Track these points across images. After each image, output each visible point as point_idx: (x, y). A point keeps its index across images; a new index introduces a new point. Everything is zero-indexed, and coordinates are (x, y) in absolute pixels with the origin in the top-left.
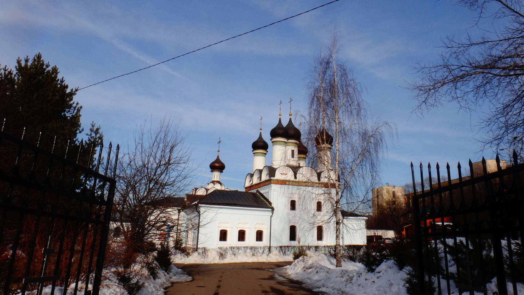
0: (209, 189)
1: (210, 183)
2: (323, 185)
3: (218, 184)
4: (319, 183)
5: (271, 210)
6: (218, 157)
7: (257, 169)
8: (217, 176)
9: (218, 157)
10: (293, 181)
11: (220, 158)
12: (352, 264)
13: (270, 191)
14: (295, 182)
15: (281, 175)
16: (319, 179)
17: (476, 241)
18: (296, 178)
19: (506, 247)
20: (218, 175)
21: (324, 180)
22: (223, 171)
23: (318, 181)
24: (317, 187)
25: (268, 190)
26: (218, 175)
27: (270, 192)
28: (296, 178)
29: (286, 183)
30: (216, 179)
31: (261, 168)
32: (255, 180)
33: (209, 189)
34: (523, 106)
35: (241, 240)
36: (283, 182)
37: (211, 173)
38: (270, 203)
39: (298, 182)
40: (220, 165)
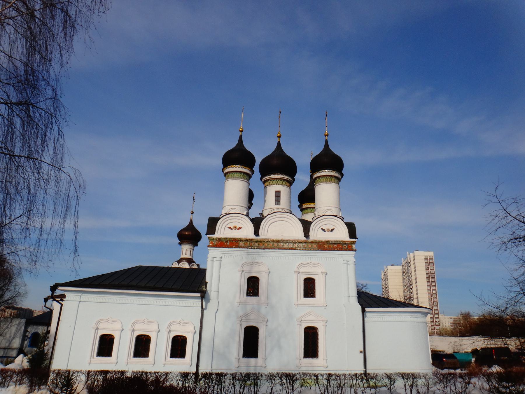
2: (315, 246)
4: (305, 242)
5: (199, 295)
6: (191, 221)
8: (187, 250)
9: (191, 221)
10: (252, 241)
11: (194, 223)
12: (25, 264)
14: (257, 241)
15: (230, 230)
16: (307, 233)
17: (495, 357)
18: (256, 233)
19: (453, 339)
20: (188, 249)
21: (316, 234)
22: (198, 243)
23: (305, 239)
24: (404, 279)
26: (188, 249)
28: (256, 233)
29: (238, 244)
30: (184, 256)
34: (1, 12)
35: (179, 356)
36: (234, 243)
37: (179, 246)
39: (262, 241)
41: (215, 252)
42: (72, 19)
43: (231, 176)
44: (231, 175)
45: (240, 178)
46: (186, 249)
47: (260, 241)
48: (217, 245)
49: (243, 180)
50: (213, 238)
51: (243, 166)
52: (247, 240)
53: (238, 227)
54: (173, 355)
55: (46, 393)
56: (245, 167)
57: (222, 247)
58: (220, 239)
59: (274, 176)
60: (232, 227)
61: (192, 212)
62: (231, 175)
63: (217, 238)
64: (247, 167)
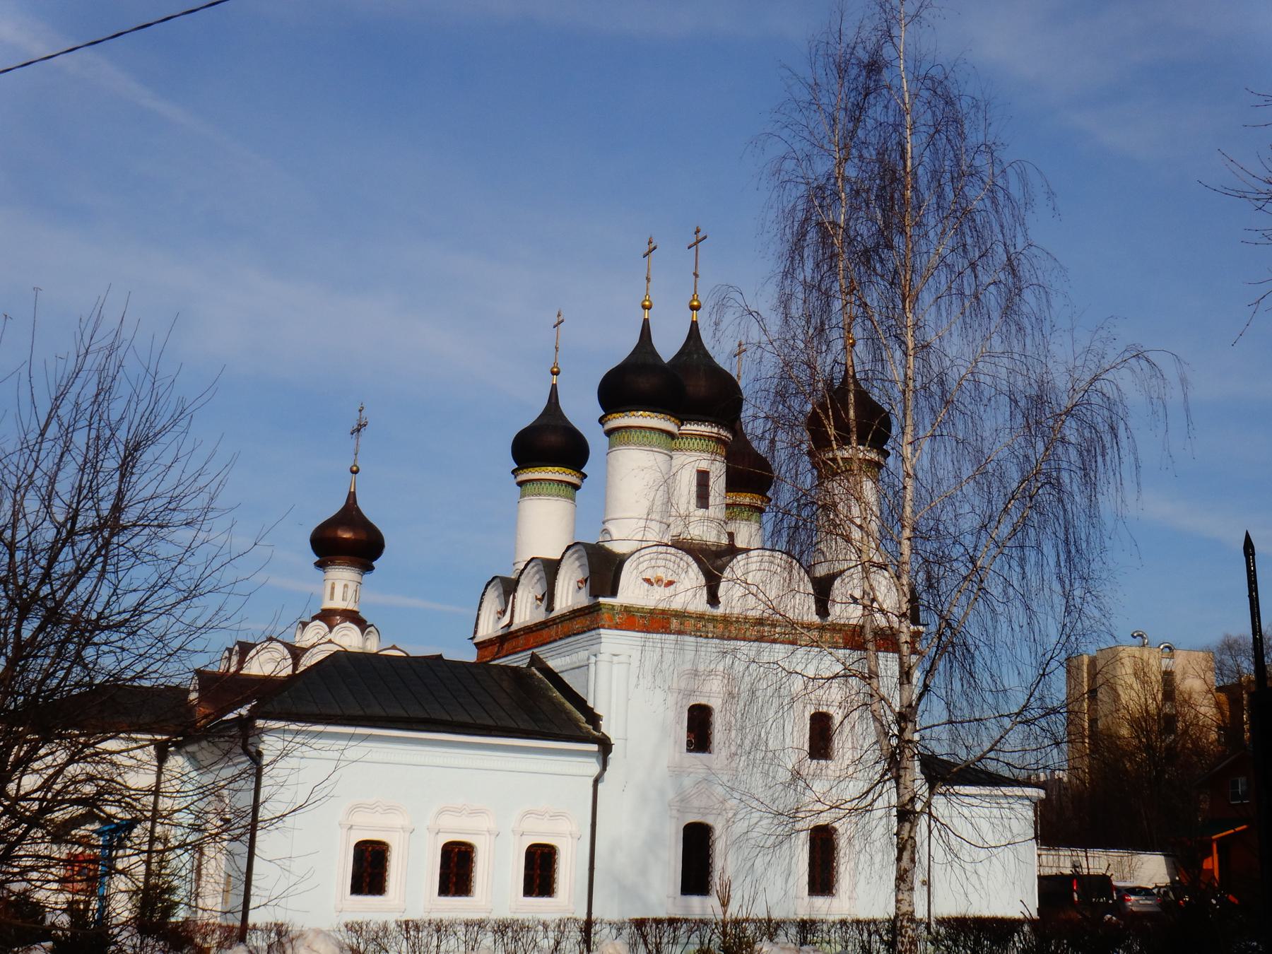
0: (305, 650)
1: (314, 618)
3: (348, 624)
5: (595, 747)
6: (352, 497)
7: (532, 559)
8: (346, 586)
9: (352, 497)
10: (701, 617)
13: (593, 659)
14: (713, 619)
16: (823, 610)
18: (713, 600)
22: (375, 563)
25: (583, 655)
27: (592, 667)
28: (713, 600)
29: (669, 623)
30: (338, 604)
31: (552, 552)
32: (526, 611)
33: (305, 650)
37: (319, 572)
38: (594, 719)
39: (726, 620)
40: (362, 536)
41: (617, 641)
42: (914, 419)
43: (635, 438)
44: (635, 437)
45: (650, 446)
46: (345, 582)
47: (695, 616)
48: (622, 624)
49: (666, 452)
50: (613, 606)
51: (669, 417)
52: (682, 615)
53: (665, 581)
54: (444, 890)
55: (138, 951)
56: (672, 419)
57: (634, 630)
58: (627, 610)
59: (695, 427)
60: (653, 580)
61: (355, 468)
62: (635, 437)
63: (622, 606)
64: (661, 413)
